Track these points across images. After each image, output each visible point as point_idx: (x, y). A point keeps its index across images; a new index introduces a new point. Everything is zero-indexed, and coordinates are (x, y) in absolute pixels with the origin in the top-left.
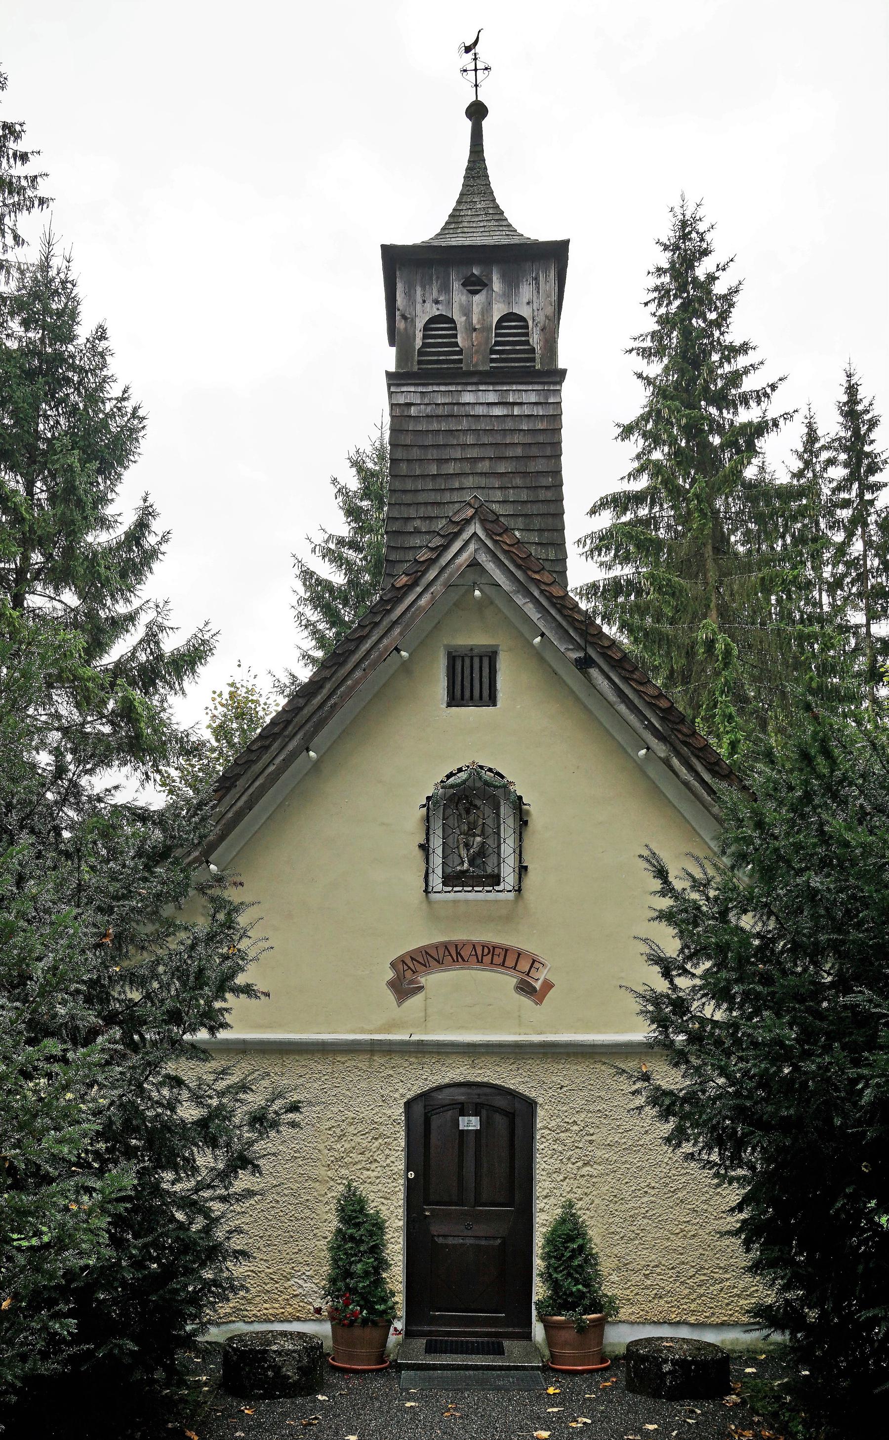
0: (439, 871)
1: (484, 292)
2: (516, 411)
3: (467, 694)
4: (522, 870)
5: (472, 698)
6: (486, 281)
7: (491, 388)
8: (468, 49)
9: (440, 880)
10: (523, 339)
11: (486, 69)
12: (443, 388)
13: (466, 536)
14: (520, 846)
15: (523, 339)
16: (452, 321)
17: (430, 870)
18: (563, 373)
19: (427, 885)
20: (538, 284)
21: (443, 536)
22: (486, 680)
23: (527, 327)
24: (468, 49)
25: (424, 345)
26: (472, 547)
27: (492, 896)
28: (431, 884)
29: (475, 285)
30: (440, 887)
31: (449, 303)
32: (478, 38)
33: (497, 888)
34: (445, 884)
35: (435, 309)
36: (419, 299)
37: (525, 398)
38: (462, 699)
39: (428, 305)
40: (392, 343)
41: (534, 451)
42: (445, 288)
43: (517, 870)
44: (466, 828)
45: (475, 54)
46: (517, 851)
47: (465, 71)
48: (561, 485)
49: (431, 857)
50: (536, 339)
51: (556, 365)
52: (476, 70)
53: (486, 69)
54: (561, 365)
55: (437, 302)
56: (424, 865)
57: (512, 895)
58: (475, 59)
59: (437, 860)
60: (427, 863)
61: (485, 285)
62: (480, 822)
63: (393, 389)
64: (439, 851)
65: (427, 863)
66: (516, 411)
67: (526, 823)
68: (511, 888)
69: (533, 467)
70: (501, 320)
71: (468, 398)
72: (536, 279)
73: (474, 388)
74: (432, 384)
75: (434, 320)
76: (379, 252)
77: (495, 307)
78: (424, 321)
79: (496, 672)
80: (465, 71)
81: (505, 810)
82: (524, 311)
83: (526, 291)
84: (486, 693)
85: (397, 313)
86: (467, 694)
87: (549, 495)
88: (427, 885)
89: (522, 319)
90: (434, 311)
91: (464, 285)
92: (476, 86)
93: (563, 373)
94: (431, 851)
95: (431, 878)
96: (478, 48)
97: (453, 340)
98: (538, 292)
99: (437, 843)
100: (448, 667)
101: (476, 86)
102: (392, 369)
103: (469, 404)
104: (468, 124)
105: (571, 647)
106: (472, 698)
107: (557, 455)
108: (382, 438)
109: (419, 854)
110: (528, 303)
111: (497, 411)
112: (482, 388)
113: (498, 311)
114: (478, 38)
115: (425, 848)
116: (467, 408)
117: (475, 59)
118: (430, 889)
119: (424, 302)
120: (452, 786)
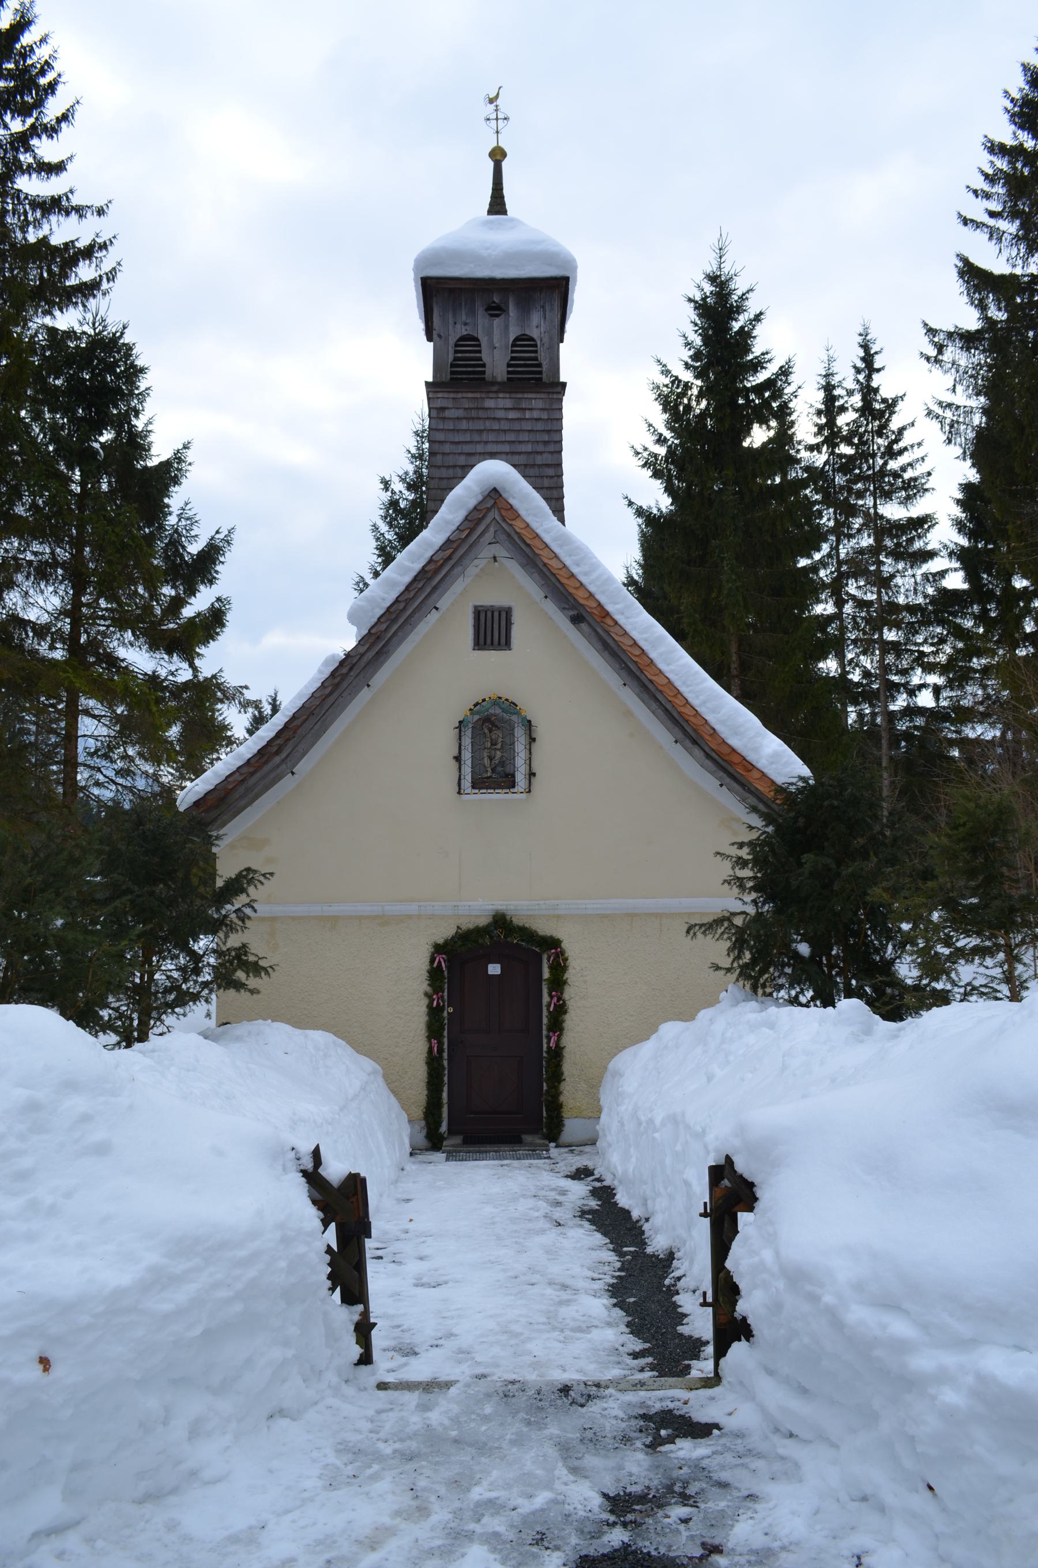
0: (469, 778)
1: (503, 316)
2: (528, 415)
3: (489, 641)
4: (532, 774)
5: (492, 644)
6: (504, 308)
7: (507, 395)
8: (491, 101)
9: (470, 785)
10: (538, 376)
11: (505, 119)
12: (470, 395)
13: (488, 520)
14: (530, 758)
15: (538, 376)
16: (477, 339)
17: (462, 777)
18: (564, 385)
19: (460, 788)
20: (544, 311)
21: (470, 521)
22: (503, 623)
23: (536, 346)
24: (491, 101)
25: (456, 359)
26: (492, 530)
27: (510, 796)
28: (462, 787)
29: (496, 310)
30: (469, 790)
31: (475, 325)
32: (498, 94)
33: (512, 790)
34: (473, 787)
35: (463, 330)
36: (451, 321)
37: (534, 404)
38: (485, 644)
39: (458, 326)
40: (430, 338)
41: (540, 448)
42: (472, 312)
43: (527, 777)
44: (489, 744)
45: (497, 106)
46: (528, 762)
47: (488, 119)
48: (562, 487)
49: (463, 767)
50: (543, 356)
51: (559, 378)
52: (497, 119)
53: (505, 119)
54: (562, 380)
55: (466, 324)
56: (457, 774)
57: (524, 795)
58: (497, 110)
59: (467, 770)
60: (460, 771)
61: (504, 311)
62: (500, 740)
63: (430, 396)
64: (469, 762)
65: (460, 771)
66: (528, 415)
67: (534, 740)
68: (523, 790)
69: (539, 460)
70: (514, 341)
71: (490, 403)
72: (543, 307)
73: (494, 395)
74: (462, 392)
75: (463, 338)
76: (373, 1235)
77: (511, 329)
78: (455, 340)
79: (511, 624)
80: (488, 119)
81: (520, 733)
82: (535, 334)
83: (536, 318)
84: (503, 640)
85: (434, 332)
86: (489, 641)
87: (550, 472)
88: (460, 788)
89: (532, 339)
90: (464, 331)
91: (486, 310)
92: (497, 132)
93: (564, 385)
94: (462, 762)
95: (462, 781)
96: (499, 102)
97: (478, 355)
98: (545, 318)
99: (467, 755)
100: (474, 626)
101: (497, 132)
102: (430, 379)
103: (490, 409)
104: (491, 164)
105: (567, 607)
106: (492, 644)
107: (560, 452)
108: (422, 410)
109: (454, 764)
110: (537, 327)
111: (512, 415)
112: (501, 395)
113: (513, 333)
114: (498, 94)
115: (458, 759)
116: (489, 411)
117: (497, 110)
118: (462, 792)
119: (455, 323)
120: (478, 713)
